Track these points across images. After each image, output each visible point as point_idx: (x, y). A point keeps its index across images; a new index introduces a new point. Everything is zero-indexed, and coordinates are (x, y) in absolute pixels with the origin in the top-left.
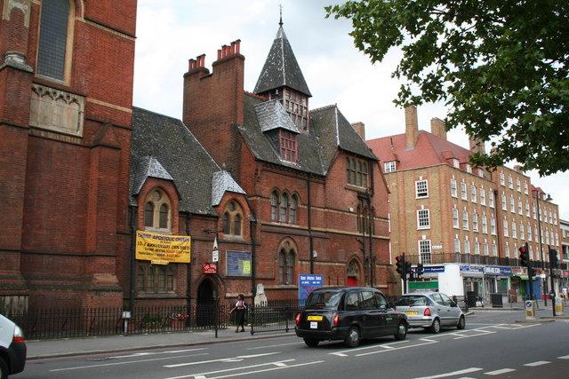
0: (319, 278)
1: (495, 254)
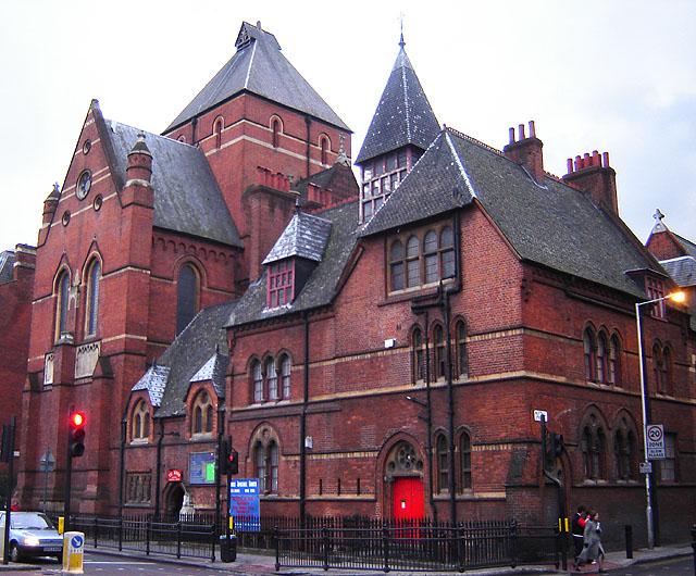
1: (452, 253)
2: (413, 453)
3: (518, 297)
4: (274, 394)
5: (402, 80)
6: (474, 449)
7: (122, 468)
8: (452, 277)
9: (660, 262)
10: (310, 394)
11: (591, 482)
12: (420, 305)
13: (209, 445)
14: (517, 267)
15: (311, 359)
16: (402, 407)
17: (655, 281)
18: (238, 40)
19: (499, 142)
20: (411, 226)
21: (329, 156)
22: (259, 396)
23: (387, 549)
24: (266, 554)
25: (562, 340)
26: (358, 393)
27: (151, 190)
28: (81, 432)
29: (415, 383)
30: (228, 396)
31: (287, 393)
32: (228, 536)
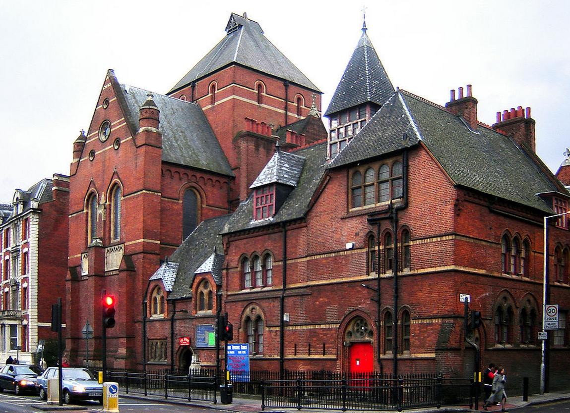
0: (244, 348)
1: (401, 181)
2: (366, 325)
3: (452, 212)
4: (259, 283)
5: (364, 55)
6: (413, 322)
7: (145, 336)
8: (400, 198)
9: (566, 187)
10: (288, 282)
11: (500, 346)
12: (374, 218)
13: (210, 320)
14: (452, 191)
15: (288, 257)
16: (359, 292)
17: (560, 200)
18: (228, 26)
19: (442, 99)
20: (368, 162)
21: (303, 110)
22: (248, 284)
23: (345, 394)
24: (254, 398)
25: (484, 243)
26: (324, 282)
27: (159, 135)
28: (111, 311)
29: (369, 275)
30: (224, 284)
31: (270, 281)
32: (226, 385)
